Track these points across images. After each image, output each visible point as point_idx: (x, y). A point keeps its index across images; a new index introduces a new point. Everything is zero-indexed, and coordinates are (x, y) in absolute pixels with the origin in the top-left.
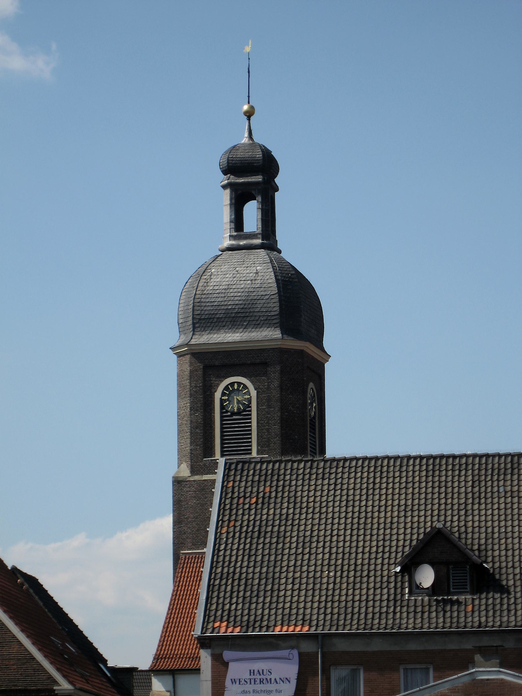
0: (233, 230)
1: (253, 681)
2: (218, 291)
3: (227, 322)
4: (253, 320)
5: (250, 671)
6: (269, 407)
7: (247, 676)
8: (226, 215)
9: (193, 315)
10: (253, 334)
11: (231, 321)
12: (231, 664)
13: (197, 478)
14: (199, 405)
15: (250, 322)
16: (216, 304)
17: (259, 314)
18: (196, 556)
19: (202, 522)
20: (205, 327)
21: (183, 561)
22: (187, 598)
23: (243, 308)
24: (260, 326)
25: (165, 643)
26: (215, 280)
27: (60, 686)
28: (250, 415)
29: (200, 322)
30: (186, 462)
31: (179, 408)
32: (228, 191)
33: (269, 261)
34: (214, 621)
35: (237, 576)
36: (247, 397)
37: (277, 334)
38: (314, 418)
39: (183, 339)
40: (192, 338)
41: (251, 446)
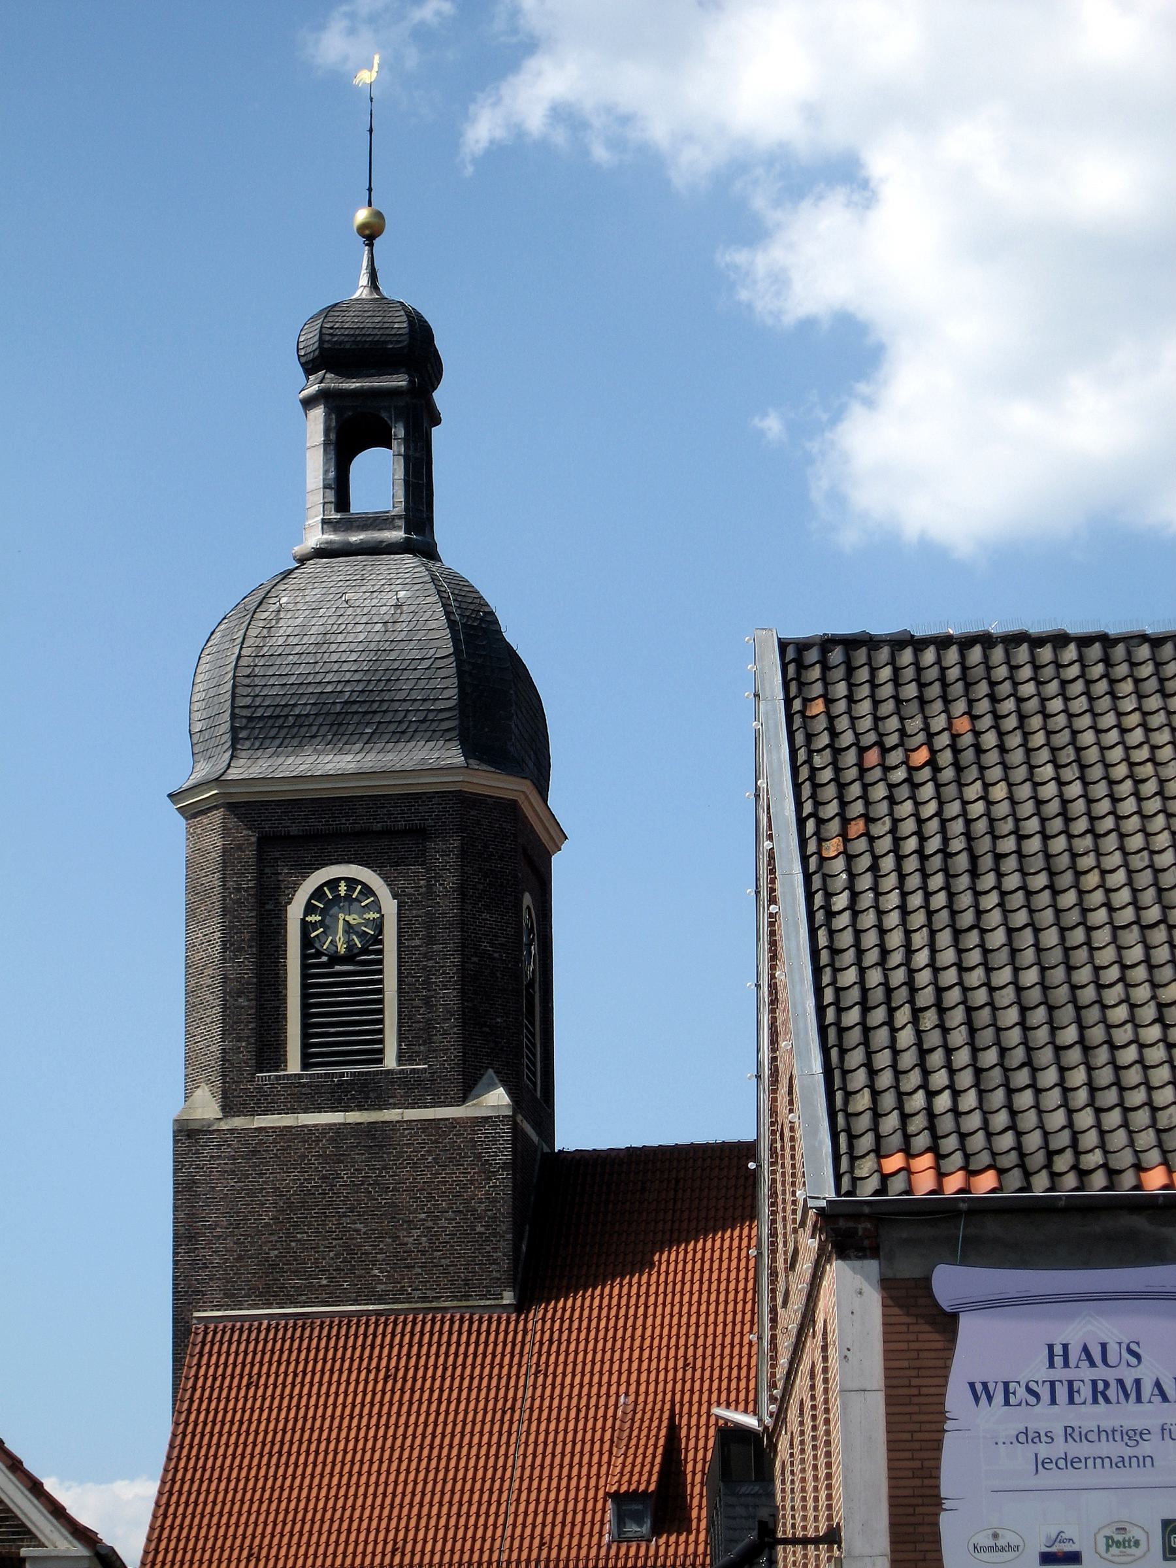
0: (332, 506)
1: (1062, 1392)
2: (297, 649)
3: (321, 725)
4: (390, 722)
5: (1051, 1347)
6: (430, 940)
7: (1038, 1371)
8: (315, 468)
9: (233, 707)
10: (390, 756)
11: (332, 725)
12: (967, 1325)
13: (238, 1122)
14: (247, 937)
15: (383, 726)
16: (292, 680)
17: (406, 706)
18: (234, 1326)
19: (252, 1238)
20: (265, 738)
21: (200, 1338)
22: (310, 1368)
23: (362, 691)
24: (408, 736)
25: (163, 1545)
26: (287, 625)
27: (43, 1546)
28: (381, 962)
29: (251, 725)
30: (208, 1082)
31: (190, 947)
32: (318, 413)
33: (428, 578)
34: (879, 1152)
35: (926, 997)
36: (372, 915)
37: (453, 755)
38: (531, 984)
39: (203, 770)
40: (229, 766)
41: (381, 1041)
